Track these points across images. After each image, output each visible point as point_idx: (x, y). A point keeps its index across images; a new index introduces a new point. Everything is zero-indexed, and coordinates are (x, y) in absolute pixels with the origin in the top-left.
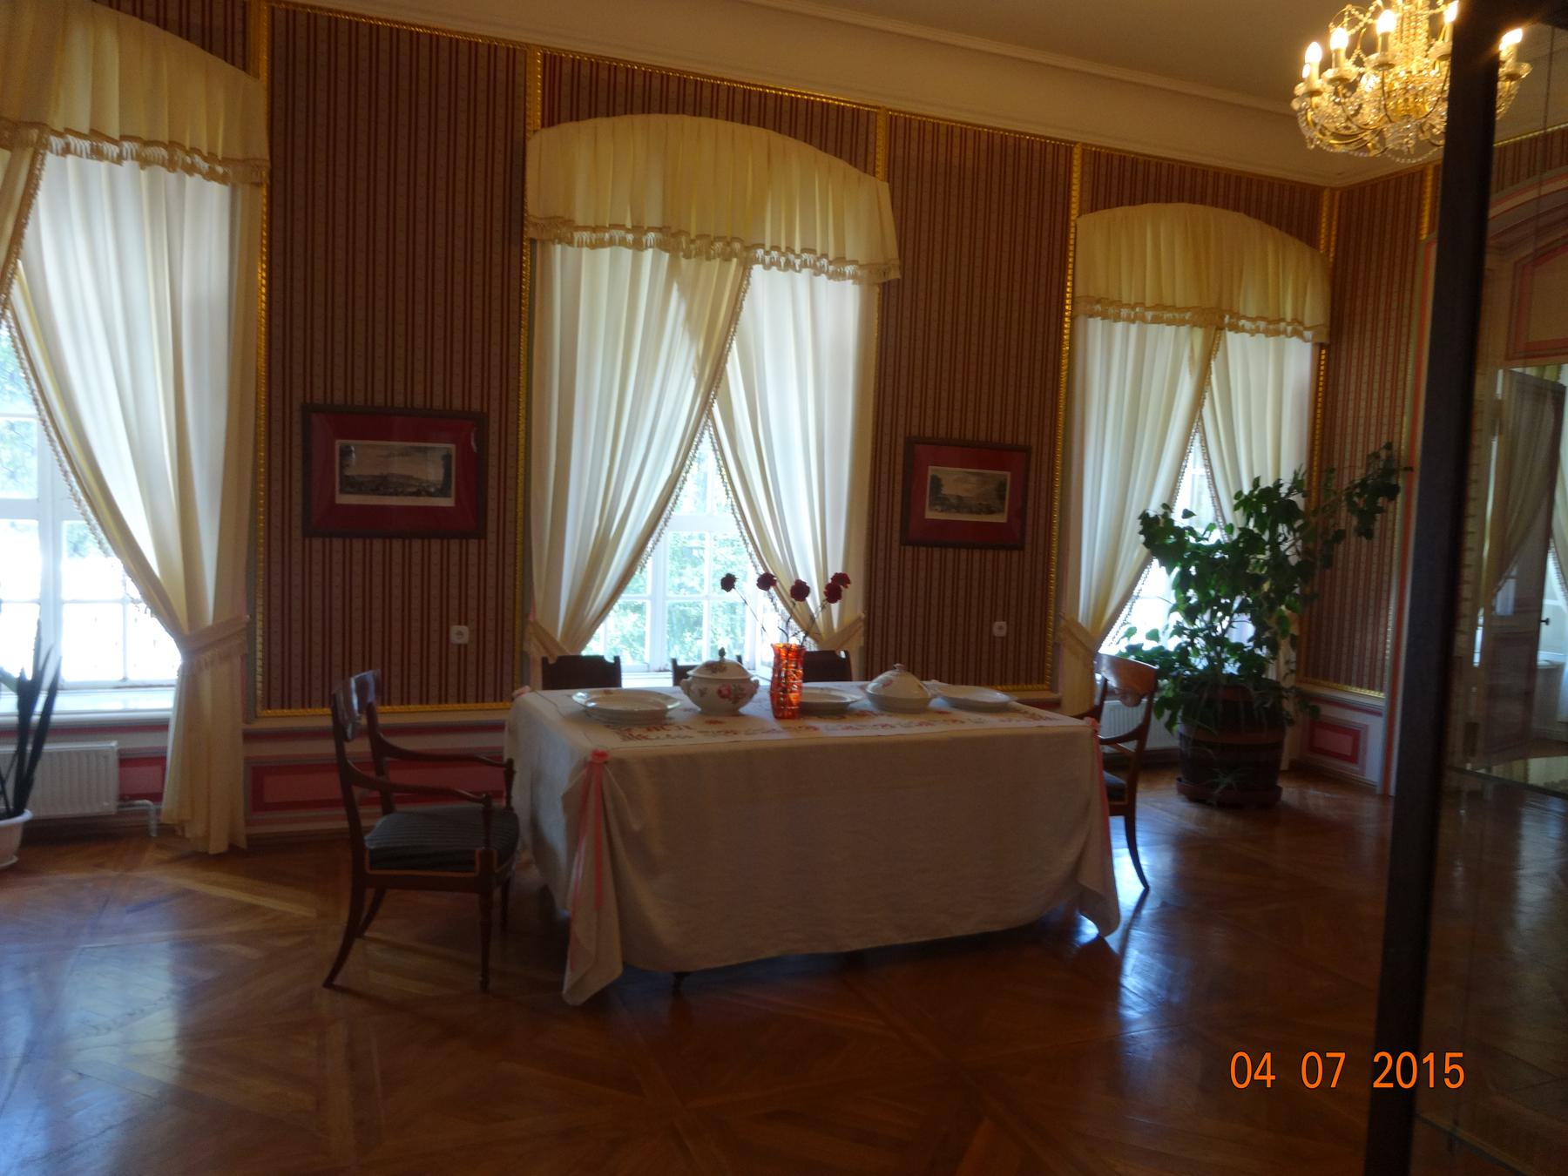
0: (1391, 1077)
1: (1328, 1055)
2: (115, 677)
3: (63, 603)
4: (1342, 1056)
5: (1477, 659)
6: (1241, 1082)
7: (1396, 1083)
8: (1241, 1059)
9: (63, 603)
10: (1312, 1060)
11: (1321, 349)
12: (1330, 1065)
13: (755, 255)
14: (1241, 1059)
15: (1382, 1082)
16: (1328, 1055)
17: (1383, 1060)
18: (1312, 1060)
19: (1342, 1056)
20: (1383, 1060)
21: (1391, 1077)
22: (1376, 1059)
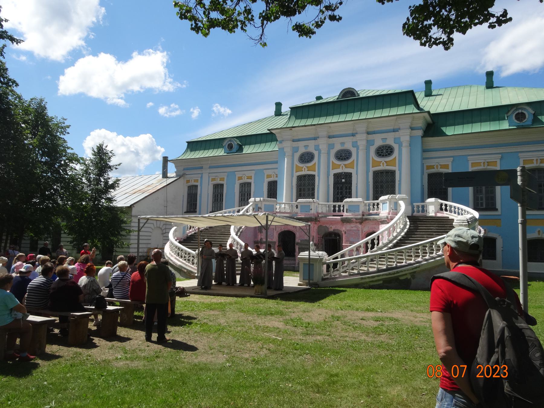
0: (483, 374)
1: (461, 366)
2: (500, 88)
3: (61, 237)
4: (466, 366)
5: (72, 314)
6: (455, 375)
7: (484, 376)
8: (455, 367)
9: (61, 237)
10: (455, 368)
11: (426, 31)
12: (461, 370)
13: (159, 50)
14: (455, 367)
15: (496, 375)
16: (461, 366)
17: (480, 367)
18: (455, 368)
19: (466, 366)
20: (480, 367)
21: (483, 374)
22: (477, 368)
